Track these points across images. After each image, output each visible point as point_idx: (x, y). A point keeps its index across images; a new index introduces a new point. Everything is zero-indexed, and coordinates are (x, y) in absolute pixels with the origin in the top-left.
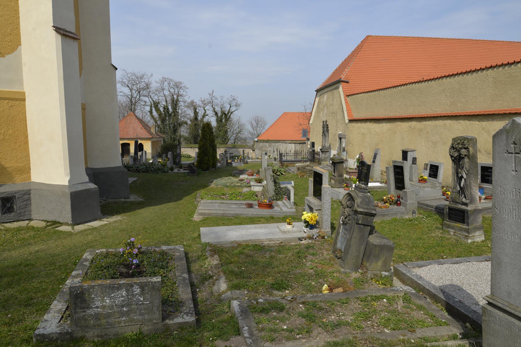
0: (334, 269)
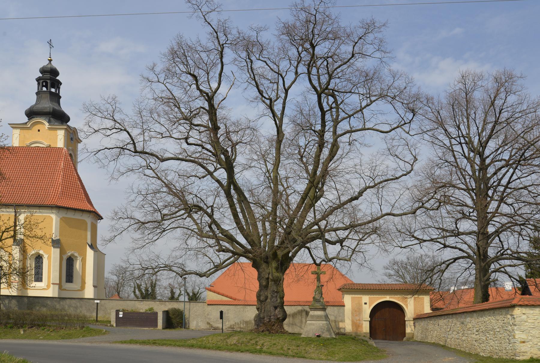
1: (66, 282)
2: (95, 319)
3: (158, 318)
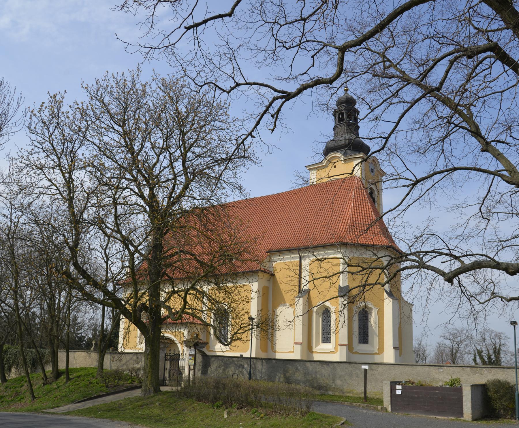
1: (360, 343)
2: (362, 396)
3: (464, 399)
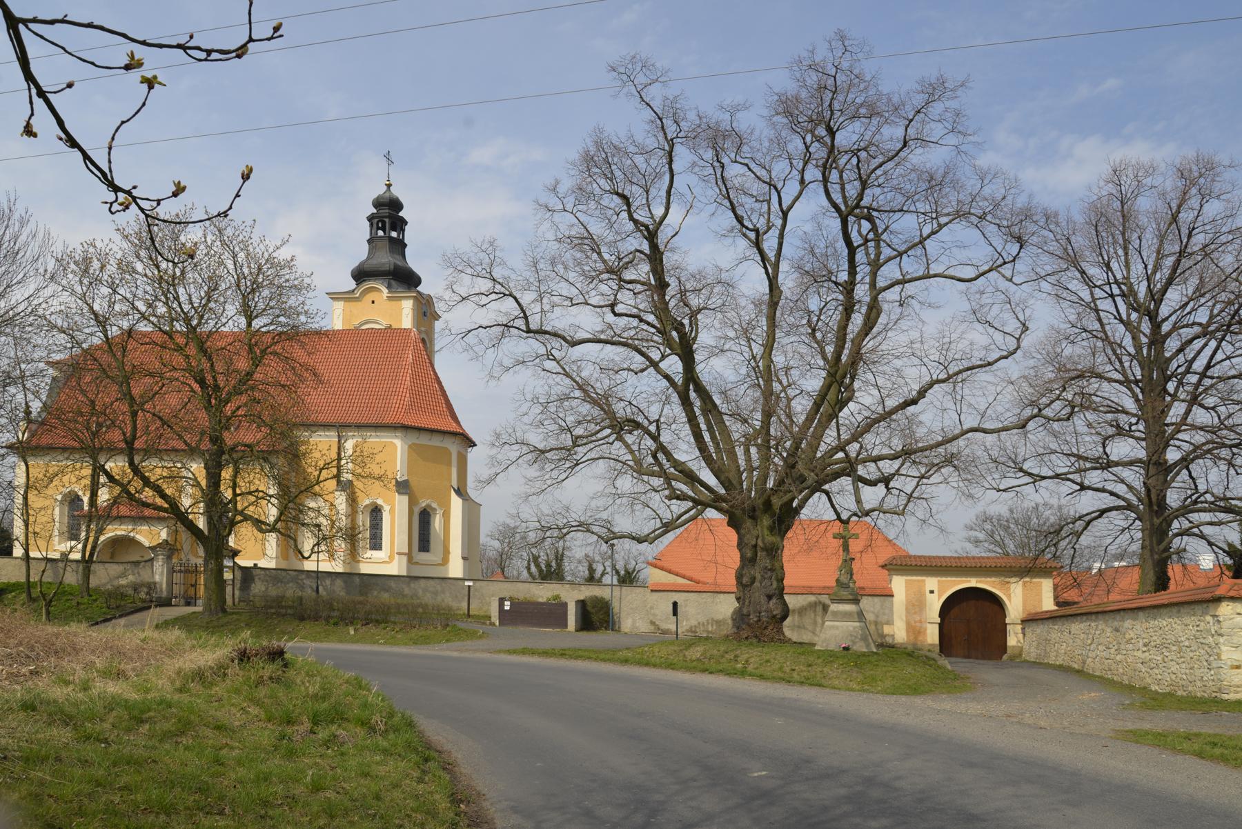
0: (1034, 515)
1: (420, 551)
